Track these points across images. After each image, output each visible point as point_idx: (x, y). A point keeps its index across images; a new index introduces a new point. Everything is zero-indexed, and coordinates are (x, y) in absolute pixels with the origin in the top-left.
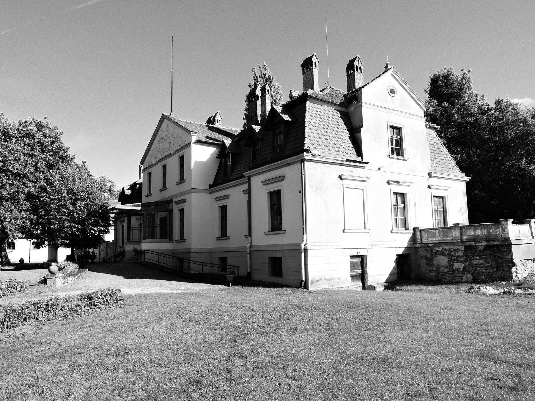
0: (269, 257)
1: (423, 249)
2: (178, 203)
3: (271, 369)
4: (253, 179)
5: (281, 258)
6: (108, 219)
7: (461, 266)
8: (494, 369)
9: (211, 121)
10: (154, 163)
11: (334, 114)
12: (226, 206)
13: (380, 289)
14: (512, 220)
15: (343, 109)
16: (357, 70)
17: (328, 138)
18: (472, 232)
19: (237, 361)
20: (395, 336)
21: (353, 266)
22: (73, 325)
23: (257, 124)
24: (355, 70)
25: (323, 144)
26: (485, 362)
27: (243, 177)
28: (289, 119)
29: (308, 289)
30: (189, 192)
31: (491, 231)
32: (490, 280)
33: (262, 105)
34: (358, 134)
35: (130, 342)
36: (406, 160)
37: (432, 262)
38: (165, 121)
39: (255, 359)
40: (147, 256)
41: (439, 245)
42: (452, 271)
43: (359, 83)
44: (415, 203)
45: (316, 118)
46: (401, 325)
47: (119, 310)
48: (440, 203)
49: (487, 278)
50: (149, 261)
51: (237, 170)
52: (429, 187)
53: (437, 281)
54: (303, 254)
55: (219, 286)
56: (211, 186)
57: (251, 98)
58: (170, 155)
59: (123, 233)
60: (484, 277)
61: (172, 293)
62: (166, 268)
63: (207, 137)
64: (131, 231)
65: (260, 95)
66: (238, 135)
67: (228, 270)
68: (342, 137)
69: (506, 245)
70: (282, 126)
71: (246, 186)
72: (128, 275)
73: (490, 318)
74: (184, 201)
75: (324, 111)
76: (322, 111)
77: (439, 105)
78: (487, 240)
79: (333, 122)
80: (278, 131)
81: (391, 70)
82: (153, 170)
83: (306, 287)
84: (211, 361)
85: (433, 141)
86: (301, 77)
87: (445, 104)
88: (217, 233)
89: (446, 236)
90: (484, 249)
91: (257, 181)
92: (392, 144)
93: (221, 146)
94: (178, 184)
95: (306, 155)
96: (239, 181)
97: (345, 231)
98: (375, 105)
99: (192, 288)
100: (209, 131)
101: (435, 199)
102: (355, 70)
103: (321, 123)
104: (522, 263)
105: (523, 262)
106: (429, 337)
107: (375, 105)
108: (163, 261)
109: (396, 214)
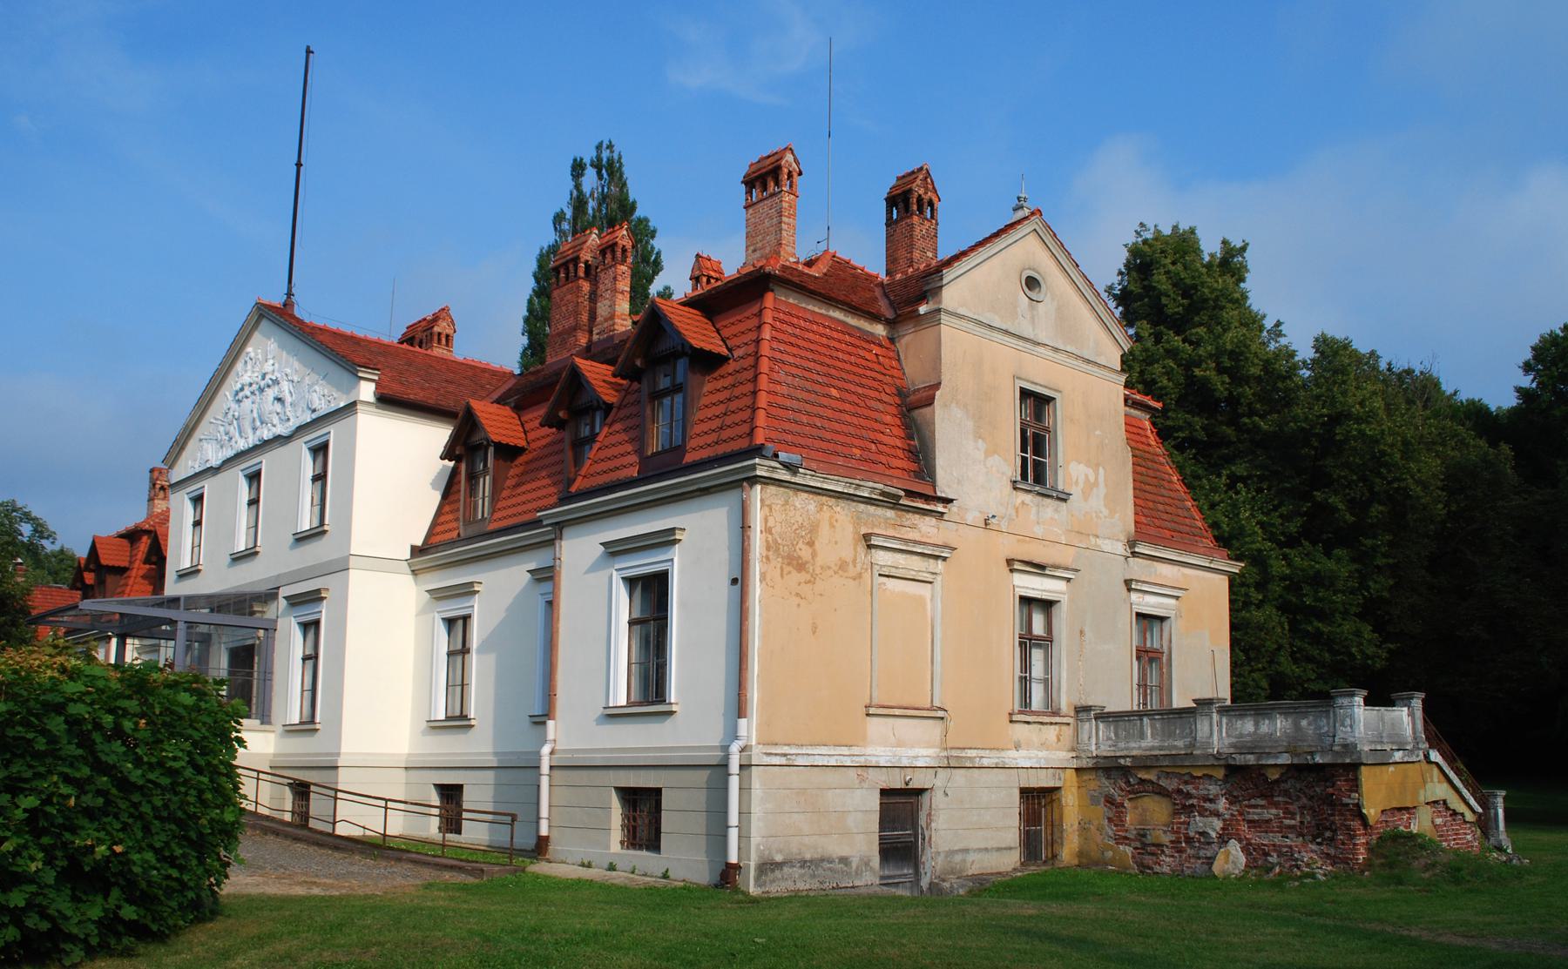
17: (829, 413)
25: (815, 432)
36: (1065, 500)
45: (795, 350)
56: (416, 551)
58: (280, 440)
69: (1344, 766)
74: (315, 597)
92: (1024, 449)
98: (980, 323)
107: (980, 323)
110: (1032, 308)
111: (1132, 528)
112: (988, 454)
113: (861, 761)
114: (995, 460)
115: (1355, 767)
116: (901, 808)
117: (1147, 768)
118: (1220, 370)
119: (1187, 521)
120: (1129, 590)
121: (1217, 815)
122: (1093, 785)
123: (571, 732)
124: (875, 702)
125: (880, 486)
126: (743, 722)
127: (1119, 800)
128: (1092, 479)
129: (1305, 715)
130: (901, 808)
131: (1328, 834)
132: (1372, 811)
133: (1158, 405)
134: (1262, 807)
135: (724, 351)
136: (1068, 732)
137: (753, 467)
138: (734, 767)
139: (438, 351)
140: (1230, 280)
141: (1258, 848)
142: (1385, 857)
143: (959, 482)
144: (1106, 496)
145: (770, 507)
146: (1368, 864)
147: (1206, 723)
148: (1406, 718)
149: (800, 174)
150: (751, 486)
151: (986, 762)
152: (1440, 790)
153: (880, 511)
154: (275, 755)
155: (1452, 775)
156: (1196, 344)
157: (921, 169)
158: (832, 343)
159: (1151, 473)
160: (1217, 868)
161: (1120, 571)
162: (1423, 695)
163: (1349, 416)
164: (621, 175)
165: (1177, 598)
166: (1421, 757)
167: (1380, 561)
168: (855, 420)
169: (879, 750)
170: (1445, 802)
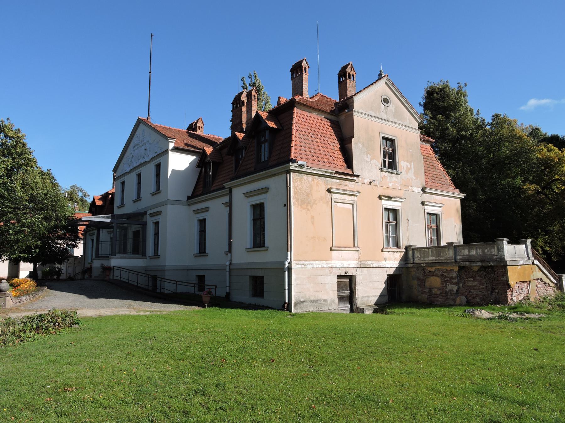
0: (250, 276)
1: (415, 269)
2: (152, 215)
3: (236, 411)
4: (234, 191)
5: (263, 277)
6: (77, 231)
7: (455, 288)
8: (493, 408)
9: (192, 127)
10: (128, 171)
11: (324, 122)
12: (205, 220)
13: (368, 312)
14: (508, 240)
15: (333, 118)
16: (350, 78)
17: (316, 147)
18: (466, 252)
19: (198, 399)
20: (383, 368)
21: (340, 287)
22: (10, 354)
23: (241, 131)
24: (348, 77)
25: (311, 154)
26: (483, 398)
27: (224, 188)
28: (275, 127)
29: (291, 311)
30: (164, 204)
31: (486, 251)
32: (483, 303)
33: (247, 112)
34: (348, 145)
35: (74, 375)
36: (399, 174)
37: (425, 283)
38: (142, 126)
39: (220, 397)
40: (117, 273)
41: (432, 265)
42: (446, 294)
43: (351, 92)
44: (408, 220)
45: (303, 126)
46: (390, 354)
47: (71, 335)
48: (433, 221)
49: (481, 301)
50: (119, 278)
51: (219, 180)
52: (423, 203)
53: (429, 304)
54: (287, 273)
55: (193, 307)
56: (189, 198)
57: (237, 103)
58: (145, 163)
59: (93, 247)
60: (478, 300)
61: (139, 316)
62: (137, 286)
63: (187, 144)
64: (100, 245)
65: (245, 101)
66: (221, 143)
67: (206, 290)
68: (331, 147)
69: (501, 266)
70: (267, 133)
71: (226, 199)
72: (91, 294)
73: (486, 346)
74: (159, 213)
75: (313, 119)
76: (311, 119)
77: (434, 118)
78: (482, 261)
79: (322, 131)
80: (263, 139)
81: (385, 78)
82: (126, 179)
83: (289, 309)
84: (167, 399)
85: (427, 155)
86: (290, 82)
87: (440, 116)
88: (196, 250)
89: (440, 256)
90: (479, 269)
91: (238, 193)
92: (384, 157)
93: (202, 155)
94: (153, 194)
95: (292, 166)
96: (221, 193)
97: (333, 248)
98: (367, 115)
99: (163, 309)
100: (189, 138)
101: (429, 216)
102: (348, 77)
103: (309, 131)
104: (517, 285)
105: (519, 284)
106: (421, 368)
107: (367, 115)
108: (133, 280)
109: (387, 232)
110: (385, 109)
112: (371, 159)
114: (374, 161)
119: (445, 180)
128: (409, 166)
132: (512, 283)
143: (362, 169)
144: (414, 173)
151: (374, 266)
157: (349, 64)
159: (431, 164)
169: (337, 262)
170: (541, 279)
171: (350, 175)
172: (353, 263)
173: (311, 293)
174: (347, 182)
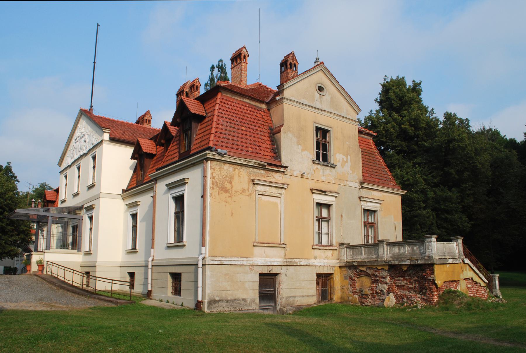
10: (70, 164)
16: (291, 68)
17: (240, 136)
25: (234, 142)
36: (334, 168)
44: (341, 216)
45: (228, 113)
56: (124, 191)
85: (368, 149)
92: (318, 148)
102: (289, 66)
110: (320, 98)
111: (362, 178)
112: (302, 150)
113: (251, 263)
114: (305, 153)
115: (432, 265)
116: (268, 282)
117: (363, 266)
118: (411, 125)
120: (361, 200)
121: (386, 283)
122: (345, 272)
123: (160, 254)
124: (257, 241)
125: (257, 161)
126: (203, 248)
127: (353, 278)
128: (345, 160)
129: (416, 245)
130: (268, 282)
131: (424, 291)
132: (439, 282)
133: (375, 134)
134: (401, 280)
135: (205, 114)
136: (336, 253)
137: (206, 154)
138: (200, 265)
139: (146, 126)
140: (415, 94)
141: (400, 296)
142: (444, 300)
143: (291, 161)
144: (351, 166)
145: (214, 169)
146: (438, 302)
147: (382, 249)
148: (456, 247)
149: (248, 56)
150: (207, 161)
151: (302, 264)
152: (470, 274)
153: (259, 171)
154: (82, 262)
155: (474, 268)
156: (403, 117)
158: (244, 111)
159: (372, 158)
160: (386, 303)
161: (357, 193)
162: (462, 238)
163: (455, 140)
164: (225, 70)
165: (380, 204)
166: (461, 261)
167: (468, 192)
168: (251, 138)
170: (472, 278)
171: (277, 166)
172: (277, 261)
173: (229, 292)
174: (273, 174)
